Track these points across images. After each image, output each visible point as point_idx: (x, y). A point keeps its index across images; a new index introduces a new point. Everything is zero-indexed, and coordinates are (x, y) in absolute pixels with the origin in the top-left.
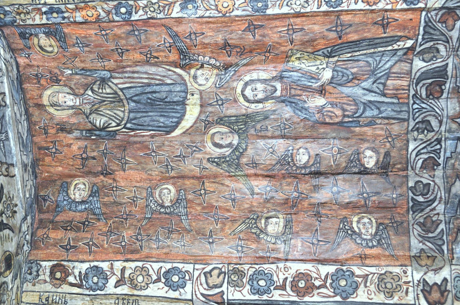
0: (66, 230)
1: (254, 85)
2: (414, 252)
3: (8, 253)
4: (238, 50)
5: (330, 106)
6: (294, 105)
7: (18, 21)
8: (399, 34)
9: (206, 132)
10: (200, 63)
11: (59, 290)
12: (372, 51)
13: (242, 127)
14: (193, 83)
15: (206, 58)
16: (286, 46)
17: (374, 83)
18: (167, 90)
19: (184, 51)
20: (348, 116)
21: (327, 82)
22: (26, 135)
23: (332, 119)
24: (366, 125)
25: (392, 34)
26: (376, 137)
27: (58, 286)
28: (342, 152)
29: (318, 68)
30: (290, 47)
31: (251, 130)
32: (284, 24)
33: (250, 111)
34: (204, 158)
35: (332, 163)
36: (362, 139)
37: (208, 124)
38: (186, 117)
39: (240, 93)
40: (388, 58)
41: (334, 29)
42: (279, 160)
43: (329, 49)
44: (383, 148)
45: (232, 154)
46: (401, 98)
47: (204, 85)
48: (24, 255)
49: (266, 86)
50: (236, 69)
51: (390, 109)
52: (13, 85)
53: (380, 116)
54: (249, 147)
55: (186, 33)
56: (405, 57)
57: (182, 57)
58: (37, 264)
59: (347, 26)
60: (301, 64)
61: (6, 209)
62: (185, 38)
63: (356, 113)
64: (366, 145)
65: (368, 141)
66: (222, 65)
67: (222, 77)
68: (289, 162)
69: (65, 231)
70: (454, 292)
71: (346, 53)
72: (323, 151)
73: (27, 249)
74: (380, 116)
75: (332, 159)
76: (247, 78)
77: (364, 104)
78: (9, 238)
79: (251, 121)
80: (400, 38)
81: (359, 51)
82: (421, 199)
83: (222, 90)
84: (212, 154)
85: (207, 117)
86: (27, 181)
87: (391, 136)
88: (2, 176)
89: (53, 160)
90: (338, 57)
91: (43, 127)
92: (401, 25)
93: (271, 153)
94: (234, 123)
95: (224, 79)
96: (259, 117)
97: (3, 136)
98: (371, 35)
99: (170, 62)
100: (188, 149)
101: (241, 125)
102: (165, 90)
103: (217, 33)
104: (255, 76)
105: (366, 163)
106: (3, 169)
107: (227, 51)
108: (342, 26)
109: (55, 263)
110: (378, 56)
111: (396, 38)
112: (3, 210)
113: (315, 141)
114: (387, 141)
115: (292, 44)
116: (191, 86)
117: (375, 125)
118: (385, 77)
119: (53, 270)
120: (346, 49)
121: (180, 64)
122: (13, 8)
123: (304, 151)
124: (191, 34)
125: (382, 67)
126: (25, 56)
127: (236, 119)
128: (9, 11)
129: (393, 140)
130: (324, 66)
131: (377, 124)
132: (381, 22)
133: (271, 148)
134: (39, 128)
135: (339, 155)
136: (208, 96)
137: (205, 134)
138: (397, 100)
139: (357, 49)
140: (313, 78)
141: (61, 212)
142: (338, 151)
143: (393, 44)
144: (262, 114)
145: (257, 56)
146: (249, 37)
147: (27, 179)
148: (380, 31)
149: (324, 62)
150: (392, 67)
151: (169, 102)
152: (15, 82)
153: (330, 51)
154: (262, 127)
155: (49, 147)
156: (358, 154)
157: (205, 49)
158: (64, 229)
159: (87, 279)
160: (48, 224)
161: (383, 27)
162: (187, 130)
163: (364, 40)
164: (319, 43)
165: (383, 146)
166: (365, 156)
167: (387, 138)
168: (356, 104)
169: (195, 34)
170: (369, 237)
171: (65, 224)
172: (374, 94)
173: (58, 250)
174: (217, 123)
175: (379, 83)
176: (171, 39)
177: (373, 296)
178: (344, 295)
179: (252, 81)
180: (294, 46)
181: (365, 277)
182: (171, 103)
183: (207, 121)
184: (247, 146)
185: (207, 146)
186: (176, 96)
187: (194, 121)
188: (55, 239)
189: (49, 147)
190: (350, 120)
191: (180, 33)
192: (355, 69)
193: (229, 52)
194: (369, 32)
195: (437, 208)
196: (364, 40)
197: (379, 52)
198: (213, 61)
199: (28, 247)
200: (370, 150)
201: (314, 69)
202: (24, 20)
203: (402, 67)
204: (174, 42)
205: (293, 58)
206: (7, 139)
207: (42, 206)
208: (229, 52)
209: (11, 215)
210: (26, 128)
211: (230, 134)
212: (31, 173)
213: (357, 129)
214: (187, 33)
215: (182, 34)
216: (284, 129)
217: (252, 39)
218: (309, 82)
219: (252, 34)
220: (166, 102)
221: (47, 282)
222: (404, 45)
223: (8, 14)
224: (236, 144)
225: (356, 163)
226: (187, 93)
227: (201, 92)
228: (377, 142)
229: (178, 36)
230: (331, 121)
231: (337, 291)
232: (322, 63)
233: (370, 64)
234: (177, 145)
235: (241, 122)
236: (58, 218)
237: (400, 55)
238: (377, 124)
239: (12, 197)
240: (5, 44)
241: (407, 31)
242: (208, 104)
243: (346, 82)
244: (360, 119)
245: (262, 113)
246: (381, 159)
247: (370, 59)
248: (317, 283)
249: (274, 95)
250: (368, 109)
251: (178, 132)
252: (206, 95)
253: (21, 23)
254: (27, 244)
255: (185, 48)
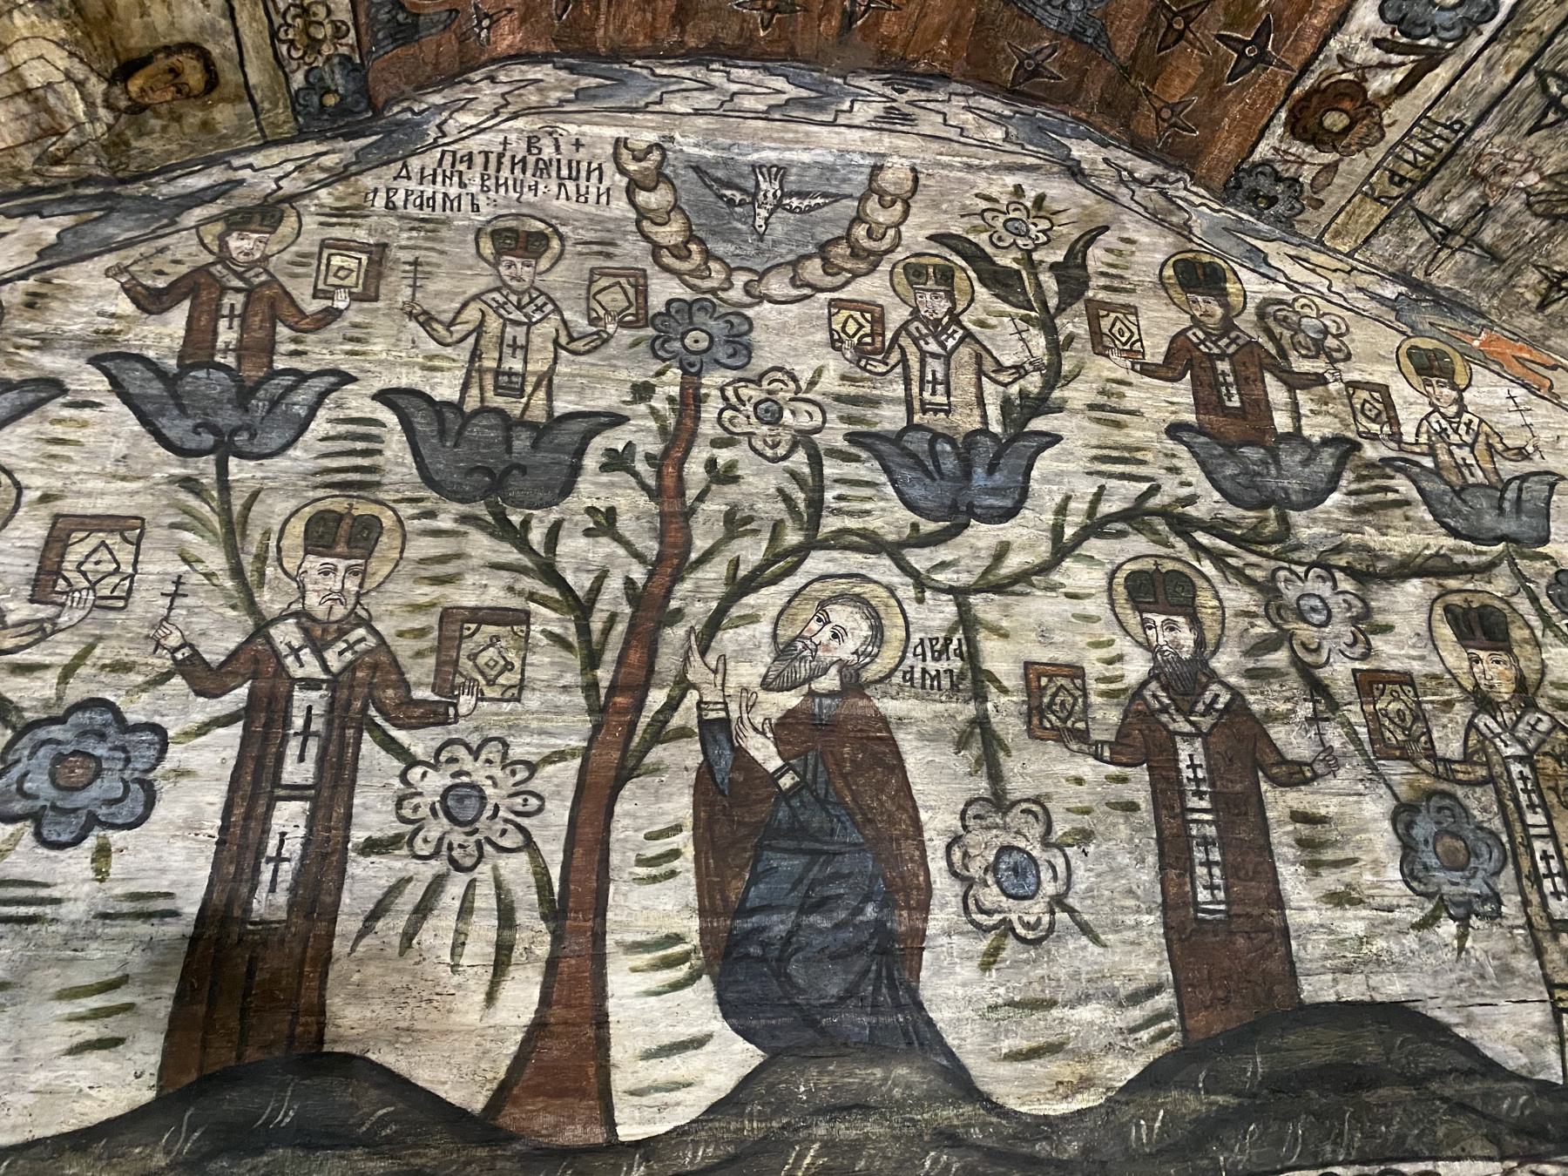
0: (1181, 35)
3: (1169, 272)
7: (344, 50)
11: (1393, 135)
22: (779, 83)
27: (1378, 135)
48: (1198, 201)
52: (594, 97)
58: (1249, 172)
61: (1020, 242)
69: (1183, 43)
73: (1181, 184)
78: (1120, 253)
86: (945, 123)
88: (903, 228)
89: (898, 8)
91: (767, 16)
106: (881, 220)
109: (1283, 115)
112: (1019, 255)
119: (1305, 130)
122: (294, 64)
126: (488, 28)
128: (306, 77)
134: (765, 29)
141: (1104, 28)
147: (940, 119)
152: (585, 82)
155: (844, 10)
158: (1176, 42)
159: (1424, 25)
160: (1128, 88)
171: (1156, 31)
173: (1240, 93)
188: (1195, 87)
189: (844, 10)
199: (1178, 180)
202: (338, 29)
206: (780, 171)
207: (1052, 86)
209: (1044, 225)
210: (759, 76)
212: (924, 95)
221: (1336, 164)
223: (321, 79)
236: (1123, 48)
239: (984, 205)
240: (437, 99)
253: (351, 38)
254: (1164, 181)
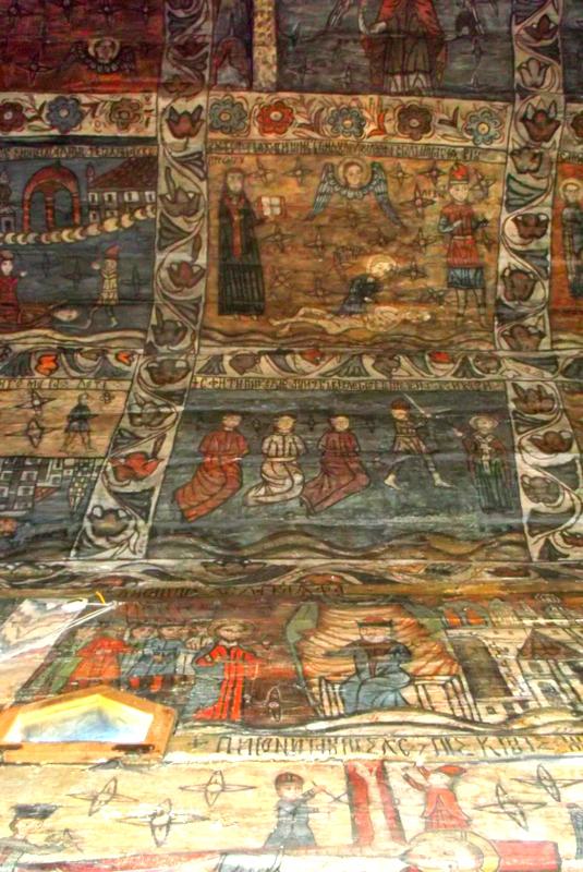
2: (165, 79)
70: (209, 121)
82: (181, 14)
170: (107, 61)
177: (102, 127)
178: (63, 128)
181: (94, 106)
195: (203, 27)
231: (55, 123)
248: (29, 114)
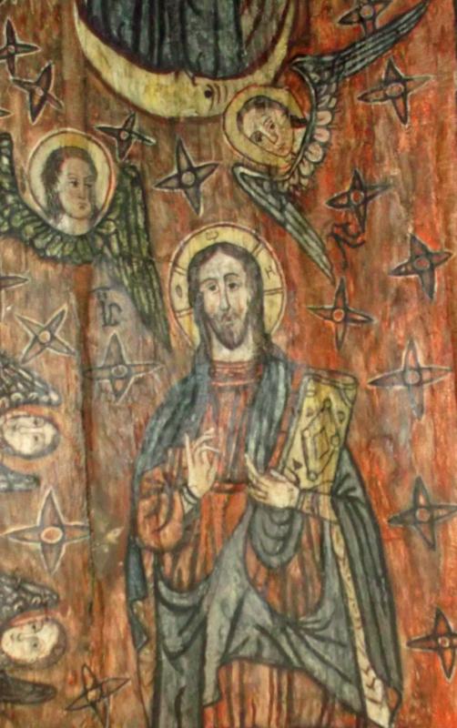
1: (244, 281)
4: (351, 228)
5: (188, 508)
6: (187, 401)
8: (407, 684)
9: (94, 134)
10: (307, 116)
12: (355, 614)
13: (115, 246)
14: (243, 97)
15: (326, 133)
16: (367, 367)
17: (262, 630)
18: (222, 15)
19: (348, 64)
20: (158, 565)
21: (260, 493)
23: (148, 516)
24: (133, 621)
25: (408, 663)
26: (100, 651)
28: (49, 555)
29: (297, 465)
30: (365, 380)
31: (105, 274)
32: (434, 355)
33: (165, 270)
34: (9, 122)
35: (12, 530)
36: (91, 610)
37: (120, 140)
38: (142, 75)
39: (219, 240)
40: (333, 661)
41: (422, 500)
42: (15, 364)
43: (358, 493)
44: (65, 680)
45: (26, 213)
46: (217, 710)
47: (241, 129)
49: (243, 316)
50: (289, 227)
51: (183, 682)
53: (164, 657)
54: (50, 269)
55: (404, 68)
56: (337, 706)
57: (328, 59)
59: (429, 538)
60: (308, 415)
62: (391, 66)
63: (169, 586)
64: (73, 627)
65: (85, 631)
66: (304, 182)
67: (266, 185)
68: (9, 395)
71: (346, 541)
72: (50, 497)
74: (164, 657)
75: (24, 527)
76: (263, 258)
77: (196, 608)
79: (133, 274)
80: (392, 684)
81: (354, 577)
83: (226, 183)
84: (24, 148)
85: (140, 137)
87: (102, 696)
90: (334, 518)
92: (436, 685)
93: (36, 338)
94: (127, 221)
95: (259, 190)
96: (147, 297)
97: (5, 143)
98: (403, 607)
99: (308, 23)
100: (38, 70)
101: (120, 244)
102: (220, 9)
103: (405, 165)
104: (273, 280)
105: (15, 631)
107: (347, 194)
108: (432, 522)
110: (337, 632)
111: (394, 676)
113: (79, 470)
114: (89, 686)
115: (373, 383)
116: (235, 92)
117: (135, 645)
118: (278, 657)
120: (359, 540)
121: (303, 56)
123: (48, 440)
124: (404, 82)
125: (308, 646)
127: (137, 227)
129: (93, 704)
130: (305, 483)
131: (138, 652)
132: (442, 628)
133: (53, 338)
135: (39, 546)
136: (205, 140)
137: (87, 128)
138: (209, 700)
139: (359, 569)
140: (270, 452)
142: (51, 545)
143: (376, 672)
144: (156, 307)
145: (334, 283)
146: (395, 258)
148: (415, 631)
149: (318, 482)
150: (308, 674)
151: (183, 21)
153: (352, 494)
154: (114, 310)
156: (44, 606)
157: (356, 127)
161: (428, 638)
162: (98, 74)
163: (389, 590)
164: (378, 462)
165: (70, 676)
166: (38, 626)
167: (96, 685)
168: (193, 586)
169: (404, 95)
172: (225, 632)
174: (122, 168)
175: (259, 644)
176: (386, 22)
179: (256, 276)
180: (369, 393)
182: (178, 27)
183: (130, 139)
184: (53, 259)
185: (50, 133)
186: (202, 42)
187: (127, 94)
190: (149, 573)
191: (407, 49)
192: (298, 571)
193: (345, 201)
194: (414, 599)
196: (390, 589)
197: (351, 634)
198: (315, 154)
200: (59, 638)
201: (297, 453)
203: (308, 703)
204: (375, 31)
205: (327, 391)
208: (345, 201)
211: (88, 208)
213: (119, 597)
214: (405, 71)
215: (401, 56)
216: (111, 378)
217: (389, 267)
218: (258, 443)
219: (405, 265)
220: (182, 11)
222: (374, 701)
224: (59, 227)
225: (15, 602)
226: (214, 77)
227: (217, 119)
228: (84, 658)
229: (395, 42)
230: (141, 517)
232: (312, 476)
233: (314, 612)
234: (49, 34)
235: (129, 241)
237: (341, 692)
238: (138, 652)
241: (416, 704)
242: (180, 143)
243: (259, 548)
244: (152, 599)
245: (160, 306)
246: (30, 676)
247: (328, 609)
249: (215, 342)
250: (183, 619)
251: (90, 44)
252: (208, 135)
255: (359, 67)
